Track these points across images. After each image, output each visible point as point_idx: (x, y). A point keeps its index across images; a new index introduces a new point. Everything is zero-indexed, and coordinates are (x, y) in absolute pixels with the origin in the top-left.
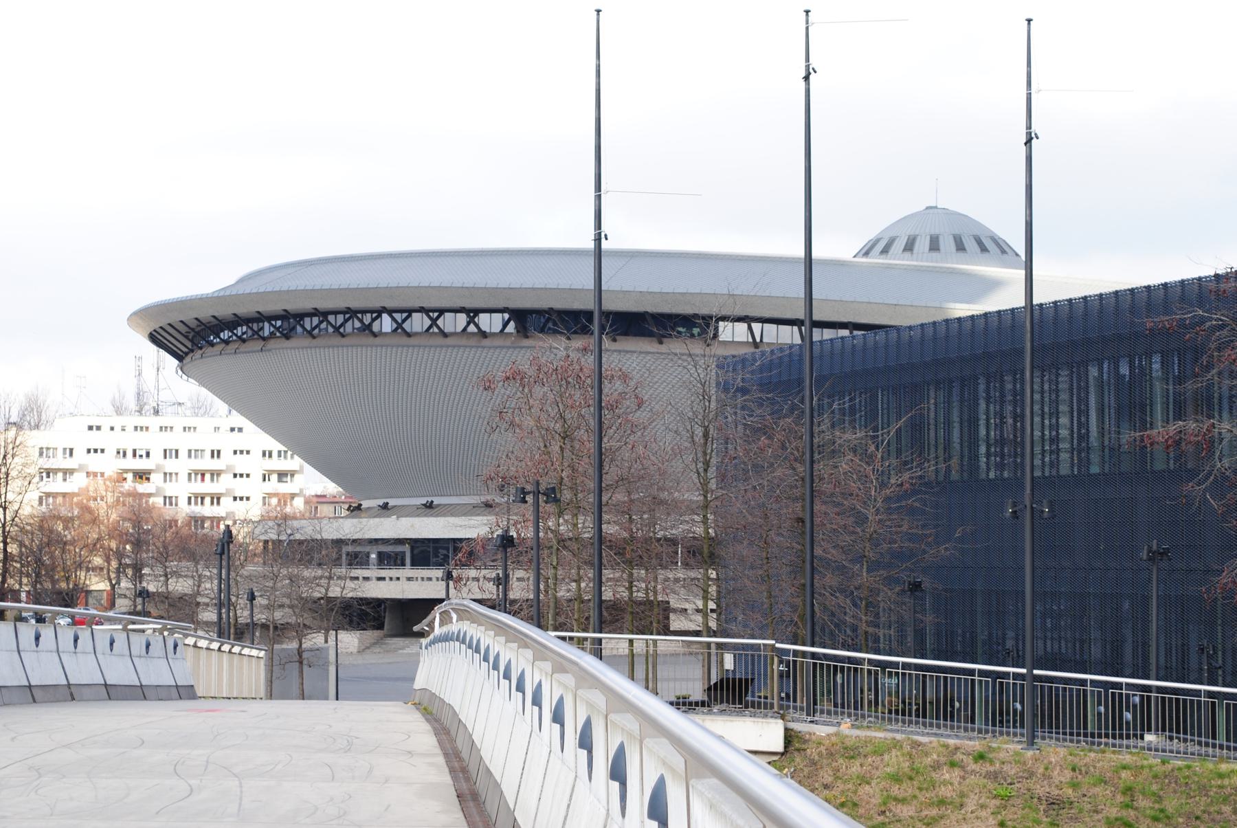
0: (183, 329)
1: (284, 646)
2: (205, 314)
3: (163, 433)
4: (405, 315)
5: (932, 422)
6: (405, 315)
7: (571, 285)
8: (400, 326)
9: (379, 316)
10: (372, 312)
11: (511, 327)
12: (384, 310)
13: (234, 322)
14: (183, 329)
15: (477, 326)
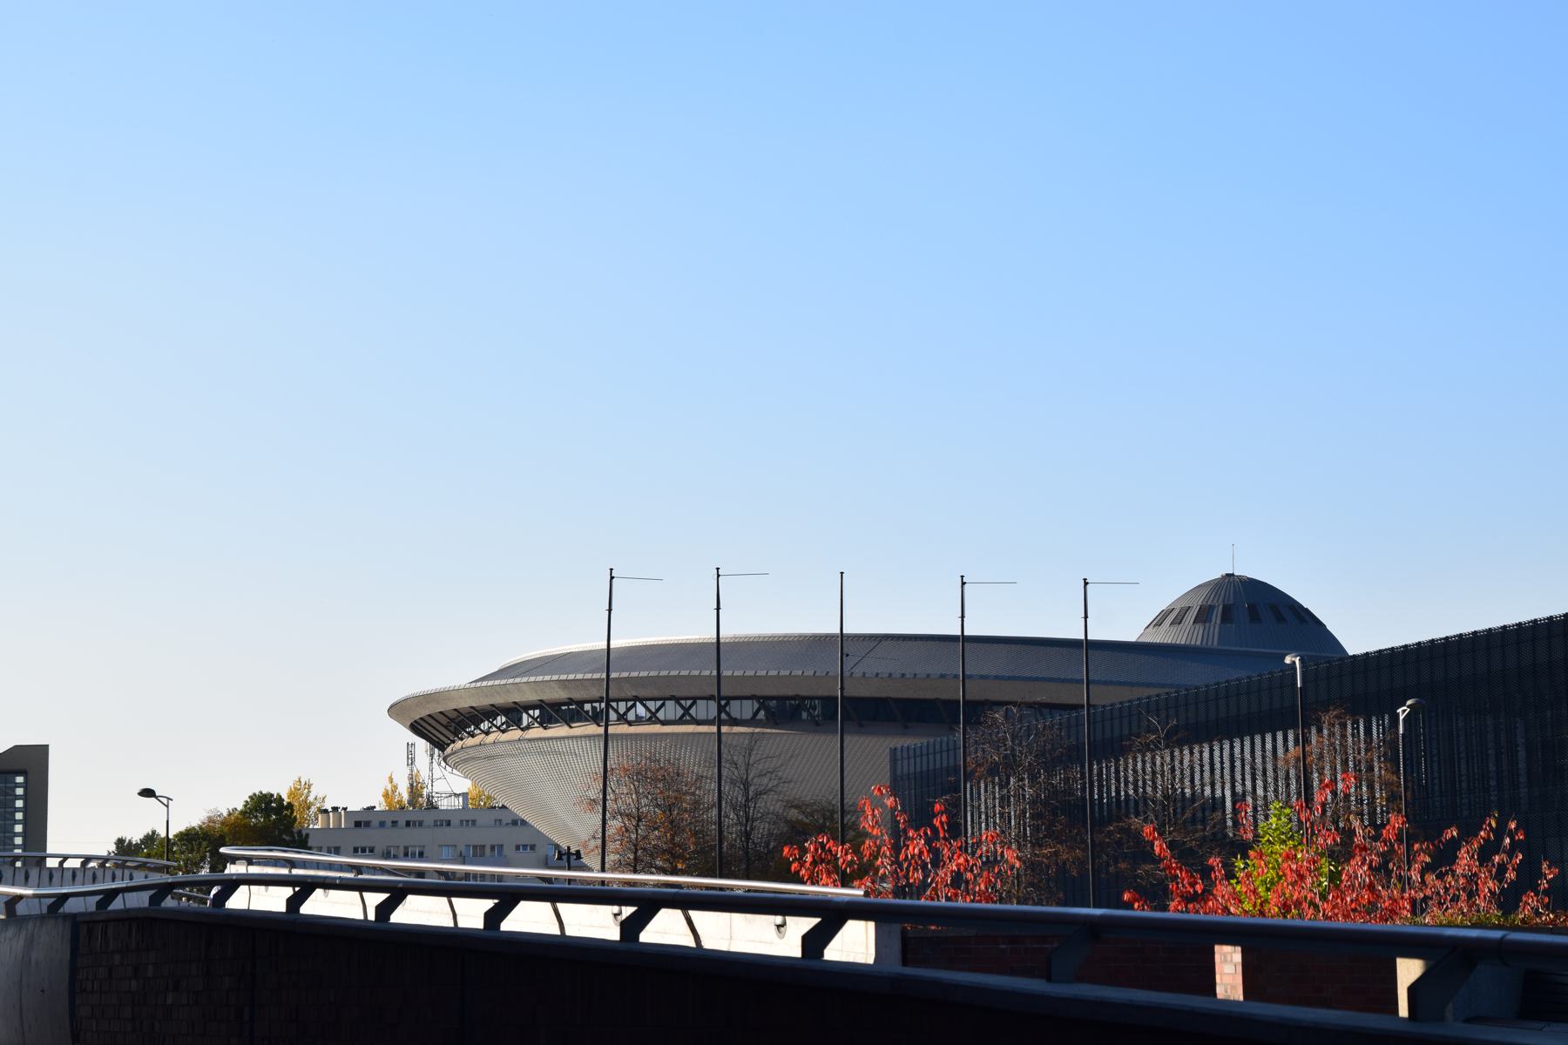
0: (444, 720)
1: (1243, 674)
2: (464, 704)
3: (359, 830)
4: (659, 703)
5: (1293, 782)
6: (659, 703)
7: (823, 678)
8: (654, 714)
9: (634, 706)
10: (627, 700)
11: (762, 715)
12: (636, 699)
13: (490, 713)
14: (444, 720)
15: (728, 714)
